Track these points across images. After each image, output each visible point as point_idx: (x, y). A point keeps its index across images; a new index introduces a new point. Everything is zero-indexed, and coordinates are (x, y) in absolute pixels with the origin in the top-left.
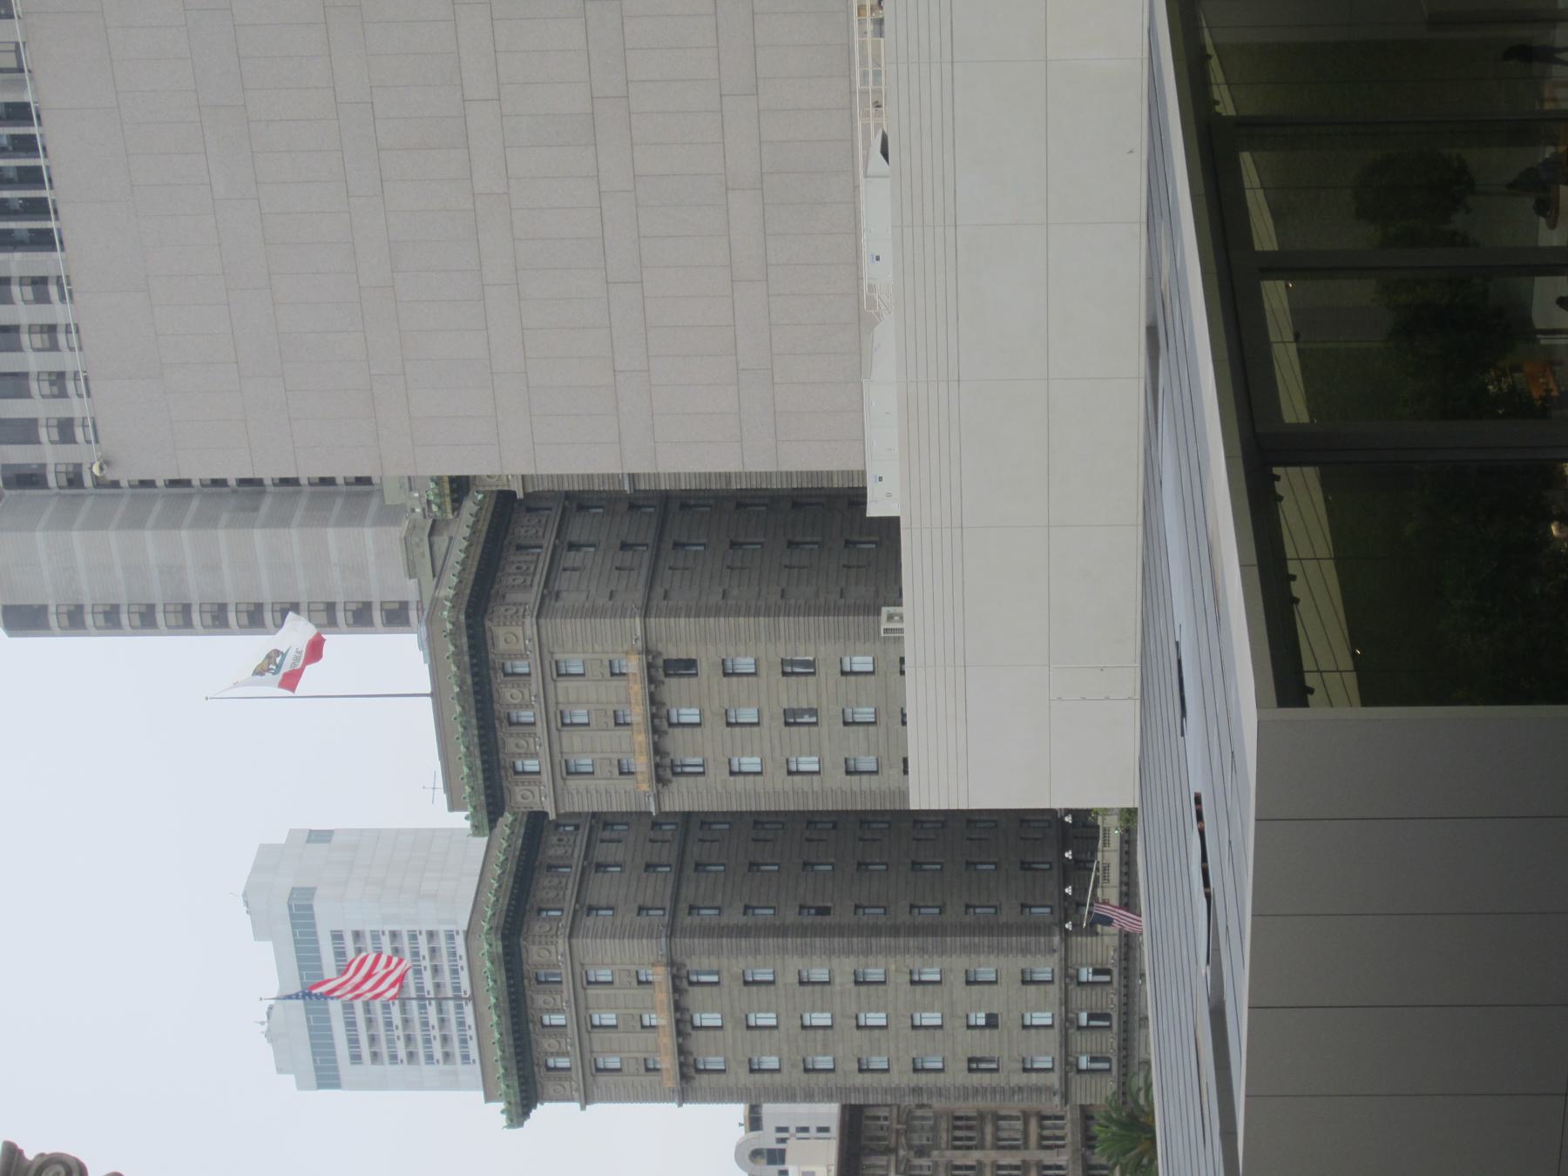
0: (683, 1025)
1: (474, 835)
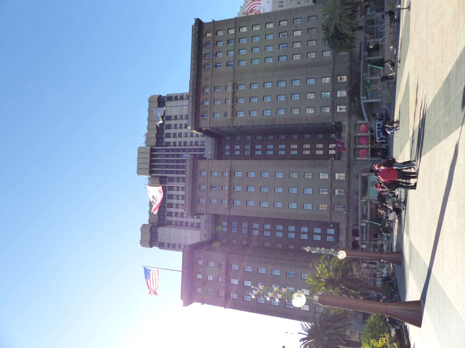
1: (184, 306)
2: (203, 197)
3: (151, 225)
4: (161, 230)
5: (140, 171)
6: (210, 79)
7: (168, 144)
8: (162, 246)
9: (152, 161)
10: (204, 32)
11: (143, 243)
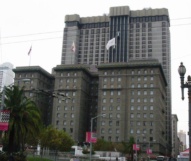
0: (67, 91)
2: (107, 74)
3: (78, 20)
4: (75, 27)
5: (112, 9)
6: (125, 75)
7: (132, 27)
8: (66, 30)
9: (119, 17)
10: (153, 69)
11: (68, 17)
